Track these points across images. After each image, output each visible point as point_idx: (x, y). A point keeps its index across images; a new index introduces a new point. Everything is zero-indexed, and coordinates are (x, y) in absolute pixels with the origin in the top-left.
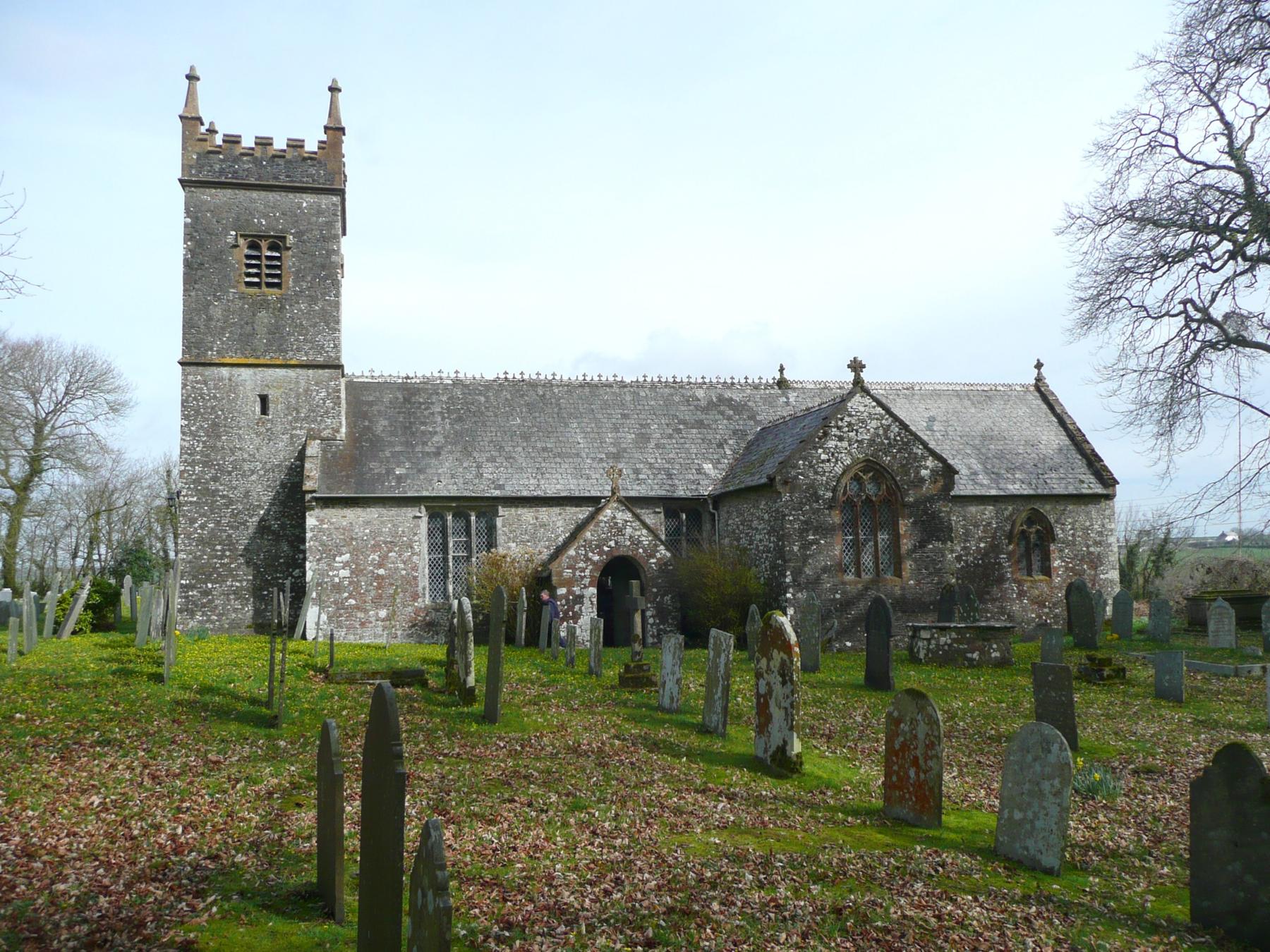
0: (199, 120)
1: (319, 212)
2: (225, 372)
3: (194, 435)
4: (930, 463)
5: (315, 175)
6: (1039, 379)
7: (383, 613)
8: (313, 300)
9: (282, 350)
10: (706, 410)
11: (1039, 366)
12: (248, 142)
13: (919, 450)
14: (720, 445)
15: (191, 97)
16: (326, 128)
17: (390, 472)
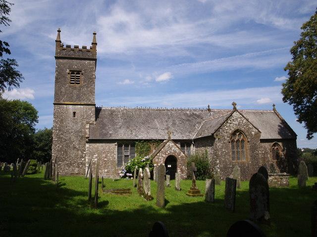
0: (60, 42)
1: (90, 65)
2: (65, 106)
3: (57, 122)
4: (254, 130)
5: (90, 55)
6: (274, 110)
7: (106, 171)
8: (87, 87)
9: (80, 101)
10: (190, 116)
11: (274, 105)
12: (80, 47)
13: (251, 126)
14: (194, 126)
15: (95, 38)
16: (92, 44)
17: (108, 132)
